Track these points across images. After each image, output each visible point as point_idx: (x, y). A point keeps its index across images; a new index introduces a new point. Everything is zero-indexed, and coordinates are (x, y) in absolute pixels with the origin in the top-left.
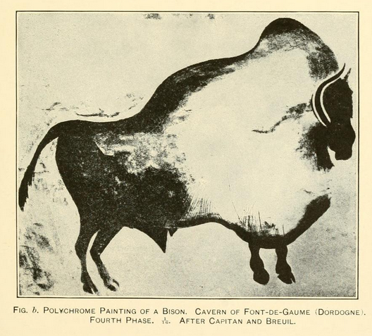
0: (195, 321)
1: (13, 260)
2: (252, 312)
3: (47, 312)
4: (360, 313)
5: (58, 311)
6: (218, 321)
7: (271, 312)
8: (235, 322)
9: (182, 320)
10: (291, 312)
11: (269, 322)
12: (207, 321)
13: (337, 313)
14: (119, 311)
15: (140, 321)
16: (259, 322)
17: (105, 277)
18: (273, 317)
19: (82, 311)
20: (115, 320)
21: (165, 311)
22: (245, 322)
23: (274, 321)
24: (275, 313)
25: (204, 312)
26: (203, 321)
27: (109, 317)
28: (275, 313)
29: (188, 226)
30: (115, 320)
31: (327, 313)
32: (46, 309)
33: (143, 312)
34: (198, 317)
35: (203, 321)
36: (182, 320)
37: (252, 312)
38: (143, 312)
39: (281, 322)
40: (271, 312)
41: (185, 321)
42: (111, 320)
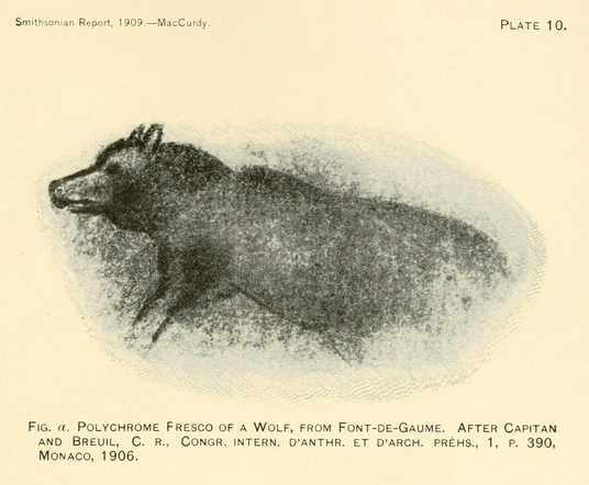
0: (481, 428)
1: (154, 122)
3: (461, 445)
5: (100, 427)
7: (381, 428)
15: (71, 457)
16: (58, 442)
19: (318, 428)
20: (324, 442)
24: (387, 429)
25: (518, 429)
28: (387, 429)
30: (324, 442)
32: (505, 23)
33: (223, 428)
38: (223, 428)
41: (467, 429)
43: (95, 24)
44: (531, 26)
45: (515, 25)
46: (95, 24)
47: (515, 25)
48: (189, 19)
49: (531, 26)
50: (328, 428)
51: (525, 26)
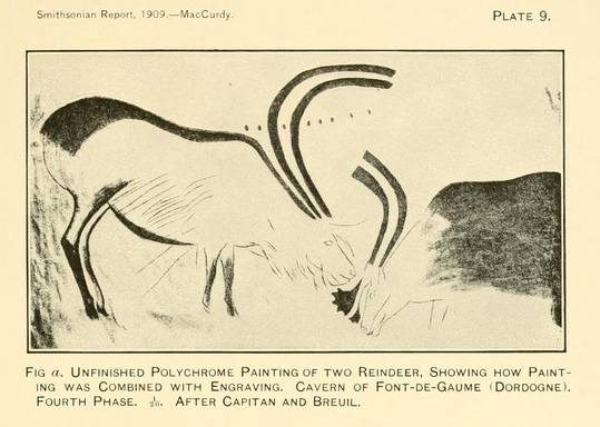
0: (199, 402)
2: (389, 387)
4: (562, 387)
5: (174, 372)
6: (237, 402)
7: (419, 388)
8: (264, 402)
9: (180, 401)
10: (451, 387)
11: (317, 403)
12: (219, 402)
13: (525, 388)
14: (271, 373)
15: (116, 402)
16: (303, 402)
17: (382, 263)
18: (324, 395)
20: (77, 402)
21: (362, 371)
22: (279, 402)
23: (327, 402)
26: (213, 402)
27: (120, 391)
29: (149, 113)
30: (192, 387)
31: (509, 388)
33: (307, 373)
34: (300, 395)
35: (213, 402)
36: (180, 401)
37: (389, 387)
38: (307, 373)
39: (337, 403)
40: (419, 388)
42: (70, 402)
43: (117, 16)
44: (524, 16)
45: (508, 16)
46: (117, 16)
47: (508, 16)
48: (212, 11)
49: (524, 16)
50: (516, 373)
51: (518, 17)
